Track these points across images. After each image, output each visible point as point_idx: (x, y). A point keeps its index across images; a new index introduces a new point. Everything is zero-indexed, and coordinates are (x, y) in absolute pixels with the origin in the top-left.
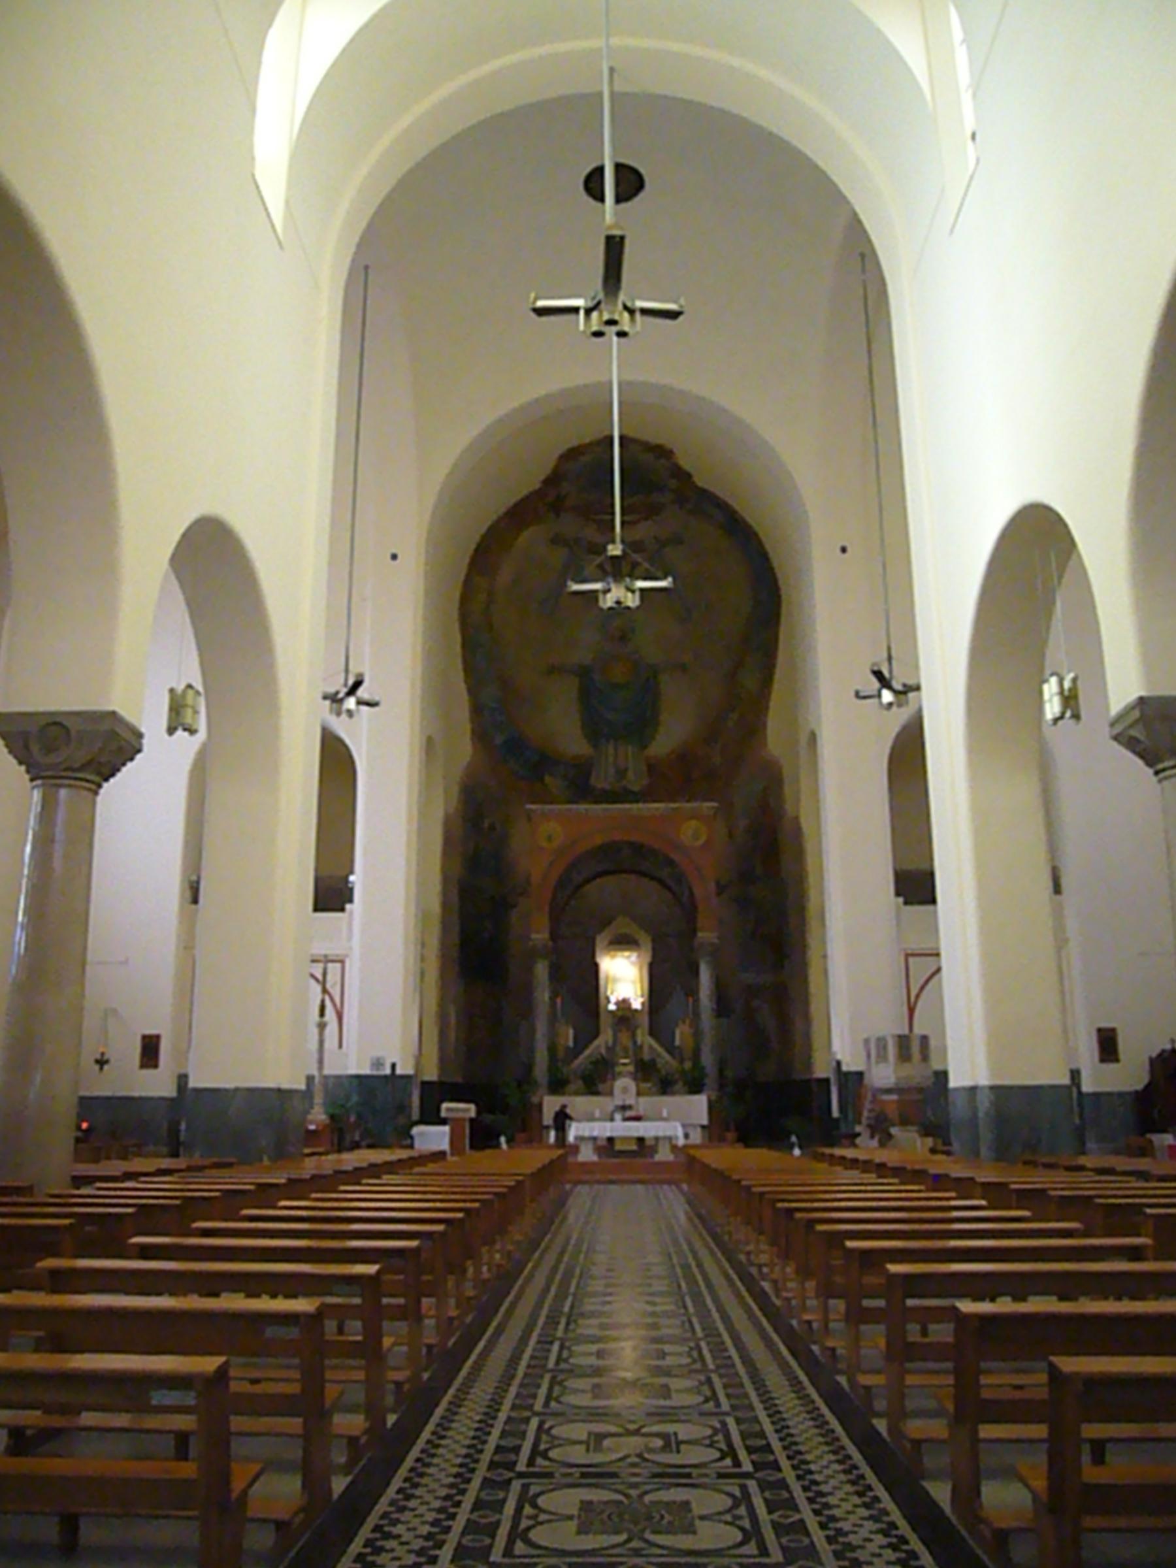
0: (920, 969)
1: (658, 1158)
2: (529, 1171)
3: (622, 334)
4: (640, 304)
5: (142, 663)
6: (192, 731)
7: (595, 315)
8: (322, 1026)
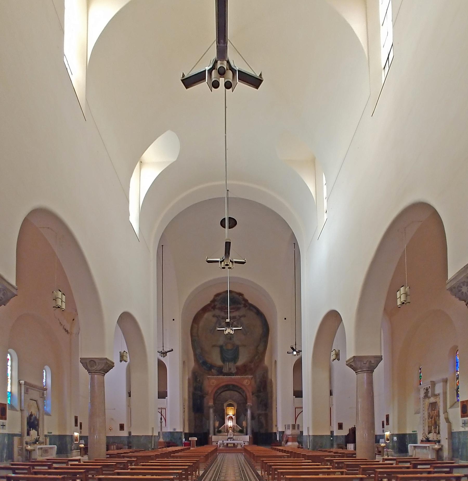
0: (298, 412)
1: (238, 448)
2: (210, 451)
3: (230, 268)
4: (234, 260)
5: (112, 346)
6: (126, 362)
7: (223, 263)
8: (161, 422)
